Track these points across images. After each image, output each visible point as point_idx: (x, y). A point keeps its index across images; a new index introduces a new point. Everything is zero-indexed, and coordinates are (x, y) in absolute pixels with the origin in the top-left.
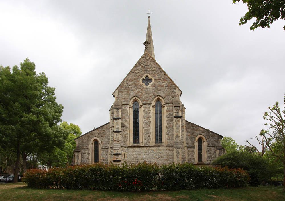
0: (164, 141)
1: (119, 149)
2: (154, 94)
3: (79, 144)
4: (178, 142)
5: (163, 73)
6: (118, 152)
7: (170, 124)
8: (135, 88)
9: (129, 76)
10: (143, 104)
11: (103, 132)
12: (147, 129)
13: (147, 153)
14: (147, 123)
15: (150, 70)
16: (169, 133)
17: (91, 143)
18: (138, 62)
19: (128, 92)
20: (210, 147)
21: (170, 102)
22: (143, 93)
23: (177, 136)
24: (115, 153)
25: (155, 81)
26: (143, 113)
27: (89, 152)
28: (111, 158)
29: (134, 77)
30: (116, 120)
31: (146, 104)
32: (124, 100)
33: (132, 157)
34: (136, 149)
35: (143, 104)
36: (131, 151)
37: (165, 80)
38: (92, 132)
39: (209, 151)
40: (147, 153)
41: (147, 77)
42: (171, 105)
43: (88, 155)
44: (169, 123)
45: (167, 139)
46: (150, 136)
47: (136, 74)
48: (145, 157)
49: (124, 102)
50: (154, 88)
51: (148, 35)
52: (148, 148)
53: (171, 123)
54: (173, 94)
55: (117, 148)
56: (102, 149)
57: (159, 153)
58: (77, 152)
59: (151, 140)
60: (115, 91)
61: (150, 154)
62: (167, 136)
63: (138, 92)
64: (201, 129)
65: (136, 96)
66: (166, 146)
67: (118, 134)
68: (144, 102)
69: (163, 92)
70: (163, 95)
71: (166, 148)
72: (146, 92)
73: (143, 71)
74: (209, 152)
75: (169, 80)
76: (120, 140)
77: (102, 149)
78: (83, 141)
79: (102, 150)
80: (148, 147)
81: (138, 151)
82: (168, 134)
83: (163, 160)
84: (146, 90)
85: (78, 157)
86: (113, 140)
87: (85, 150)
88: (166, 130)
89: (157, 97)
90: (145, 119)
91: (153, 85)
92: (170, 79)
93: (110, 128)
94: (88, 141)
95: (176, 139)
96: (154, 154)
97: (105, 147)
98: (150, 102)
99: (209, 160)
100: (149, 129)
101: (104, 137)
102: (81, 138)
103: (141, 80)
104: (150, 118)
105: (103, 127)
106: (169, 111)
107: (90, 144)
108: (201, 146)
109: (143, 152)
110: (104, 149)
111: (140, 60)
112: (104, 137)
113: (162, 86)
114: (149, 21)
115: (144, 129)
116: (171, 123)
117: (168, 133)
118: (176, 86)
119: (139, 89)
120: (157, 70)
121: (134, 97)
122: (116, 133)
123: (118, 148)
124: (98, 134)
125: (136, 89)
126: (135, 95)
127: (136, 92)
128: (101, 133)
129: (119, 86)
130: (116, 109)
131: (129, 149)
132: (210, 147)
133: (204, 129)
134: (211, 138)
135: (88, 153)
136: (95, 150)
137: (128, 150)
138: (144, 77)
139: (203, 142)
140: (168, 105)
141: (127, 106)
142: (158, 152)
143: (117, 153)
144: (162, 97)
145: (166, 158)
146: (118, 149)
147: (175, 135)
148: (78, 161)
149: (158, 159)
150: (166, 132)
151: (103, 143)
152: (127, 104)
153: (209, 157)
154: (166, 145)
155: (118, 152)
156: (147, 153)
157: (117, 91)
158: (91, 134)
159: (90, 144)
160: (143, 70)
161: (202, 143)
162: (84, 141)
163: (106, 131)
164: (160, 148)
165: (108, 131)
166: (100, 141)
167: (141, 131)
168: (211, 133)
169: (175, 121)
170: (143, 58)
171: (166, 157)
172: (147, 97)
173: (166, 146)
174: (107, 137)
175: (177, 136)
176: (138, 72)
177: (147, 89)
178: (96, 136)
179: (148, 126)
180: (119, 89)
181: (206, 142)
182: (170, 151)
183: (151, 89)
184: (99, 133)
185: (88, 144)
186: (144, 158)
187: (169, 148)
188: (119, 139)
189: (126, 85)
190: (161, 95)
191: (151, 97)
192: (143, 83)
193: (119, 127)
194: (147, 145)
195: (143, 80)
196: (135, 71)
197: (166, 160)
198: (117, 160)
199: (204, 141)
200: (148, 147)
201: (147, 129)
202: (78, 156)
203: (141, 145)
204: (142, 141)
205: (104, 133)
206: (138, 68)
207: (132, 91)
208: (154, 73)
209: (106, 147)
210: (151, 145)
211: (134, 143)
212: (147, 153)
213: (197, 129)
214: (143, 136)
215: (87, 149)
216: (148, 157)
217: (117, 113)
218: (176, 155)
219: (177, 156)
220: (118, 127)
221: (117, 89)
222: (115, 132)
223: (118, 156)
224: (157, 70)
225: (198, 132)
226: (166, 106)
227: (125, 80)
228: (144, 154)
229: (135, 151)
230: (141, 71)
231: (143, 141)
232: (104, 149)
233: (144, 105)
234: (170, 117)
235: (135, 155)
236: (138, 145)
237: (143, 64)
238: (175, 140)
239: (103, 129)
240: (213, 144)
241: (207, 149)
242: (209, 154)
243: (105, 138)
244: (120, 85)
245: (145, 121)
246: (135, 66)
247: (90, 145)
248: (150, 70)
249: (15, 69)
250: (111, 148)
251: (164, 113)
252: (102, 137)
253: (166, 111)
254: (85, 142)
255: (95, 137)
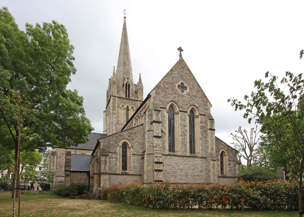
0: (198, 152)
1: (161, 157)
2: (189, 102)
3: (104, 145)
4: (213, 154)
5: (196, 84)
6: (159, 160)
7: (203, 135)
8: (172, 92)
9: (165, 78)
10: (180, 111)
11: (134, 134)
12: (183, 137)
13: (184, 164)
14: (183, 131)
15: (186, 78)
16: (203, 144)
17: (120, 146)
18: (174, 66)
19: (165, 95)
20: (230, 161)
21: (203, 114)
22: (179, 99)
23: (212, 148)
24: (156, 161)
25: (190, 90)
26: (180, 120)
27: (116, 157)
28: (147, 166)
29: (171, 80)
30: (156, 123)
31: (183, 111)
32: (161, 103)
33: (170, 166)
34: (174, 157)
35: (180, 111)
36: (168, 160)
37: (198, 91)
38: (121, 133)
39: (229, 164)
40: (184, 164)
41: (182, 83)
42: (204, 117)
43: (116, 160)
44: (202, 135)
45: (201, 150)
46: (186, 146)
47: (173, 78)
48: (182, 167)
49: (162, 105)
50: (189, 96)
51: (124, 36)
52: (185, 158)
53: (204, 134)
54: (205, 107)
55: (158, 156)
56: (133, 154)
57: (194, 164)
58: (104, 156)
59: (187, 149)
60: (152, 91)
61: (186, 164)
62: (200, 148)
63: (175, 97)
64: (223, 143)
65: (173, 101)
66: (201, 158)
67: (158, 139)
68: (181, 109)
69: (197, 102)
70: (197, 105)
71: (200, 159)
72: (182, 99)
73: (179, 77)
74: (229, 166)
75: (202, 92)
76: (160, 146)
77: (133, 154)
78: (109, 143)
79: (133, 155)
80: (184, 156)
81: (175, 160)
82: (202, 145)
83: (198, 171)
84: (182, 97)
85: (105, 162)
86: (153, 146)
87: (112, 154)
88: (200, 141)
89: (192, 107)
90: (181, 127)
91: (188, 94)
92: (202, 91)
93: (147, 132)
94: (116, 143)
95: (211, 152)
96: (190, 165)
97: (136, 153)
98: (186, 111)
99: (230, 173)
100: (185, 138)
101: (135, 141)
102: (107, 139)
103: (177, 85)
104: (186, 127)
105: (134, 129)
106: (203, 123)
107: (119, 147)
108: (223, 159)
109: (180, 161)
110: (135, 155)
111: (176, 64)
112: (135, 141)
113: (196, 96)
114: (125, 22)
115: (181, 137)
116: (204, 134)
117: (201, 144)
118: (207, 99)
119: (175, 94)
120: (191, 79)
121: (171, 101)
122: (157, 139)
123: (160, 156)
124: (127, 137)
125: (173, 94)
126: (172, 100)
127: (173, 97)
128: (132, 135)
129: (156, 86)
130: (156, 111)
131: (167, 157)
132: (230, 161)
133: (226, 144)
134: (230, 153)
135: (116, 158)
136: (122, 155)
137: (165, 158)
138: (180, 83)
139: (128, 148)
140: (201, 116)
141: (164, 109)
142: (193, 162)
143: (158, 161)
144: (178, 106)
145: (201, 170)
146: (159, 157)
147: (210, 148)
148: (105, 167)
149: (194, 170)
150: (200, 143)
151: (134, 147)
152: (165, 108)
153: (229, 170)
154: (200, 156)
155: (159, 160)
156: (183, 163)
157: (154, 91)
158: (120, 135)
159: (119, 147)
160: (179, 76)
161: (126, 150)
162: (111, 143)
163: (137, 133)
164: (195, 159)
165: (140, 134)
166: (130, 145)
167: (178, 139)
168: (230, 149)
169: (210, 133)
170: (179, 64)
171: (200, 169)
172: (184, 105)
173: (201, 158)
174: (138, 141)
175: (212, 148)
176: (175, 77)
177: (183, 96)
178: (126, 138)
179: (184, 134)
180: (156, 89)
181: (227, 156)
182: (204, 163)
183: (187, 97)
184: (129, 135)
185: (116, 147)
186: (181, 168)
187: (203, 159)
188: (159, 146)
189: (163, 86)
190: (195, 104)
191: (186, 106)
192: (179, 90)
193: (159, 131)
194: (184, 155)
195: (179, 86)
196: (172, 74)
197: (200, 171)
198: (159, 169)
199: (225, 155)
200: (184, 156)
201: (183, 137)
202: (106, 161)
203: (176, 153)
204: (178, 150)
205: (135, 136)
206: (175, 72)
207: (169, 94)
208: (189, 81)
209: (137, 152)
210: (187, 155)
211: (170, 151)
212: (183, 163)
213: (220, 143)
214: (180, 145)
215: (115, 153)
216: (184, 168)
217: (158, 116)
218: (213, 168)
219: (213, 168)
220: (158, 132)
221: (154, 89)
222: (155, 137)
223: (160, 165)
224: (191, 79)
225: (221, 146)
226: (199, 117)
227: (162, 81)
228: (181, 164)
229: (172, 160)
230: (177, 76)
231: (180, 150)
232: (135, 155)
233: (181, 112)
234: (203, 128)
235: (172, 165)
236: (174, 153)
237: (180, 70)
238: (210, 152)
239: (134, 132)
240: (232, 158)
241: (228, 163)
242: (230, 167)
243: (136, 142)
244: (157, 85)
245: (181, 128)
246: (172, 70)
247: (118, 148)
248: (186, 78)
249: (38, 25)
250: (147, 154)
251: (198, 124)
252: (132, 141)
253: (199, 122)
254: (113, 144)
255: (124, 139)
